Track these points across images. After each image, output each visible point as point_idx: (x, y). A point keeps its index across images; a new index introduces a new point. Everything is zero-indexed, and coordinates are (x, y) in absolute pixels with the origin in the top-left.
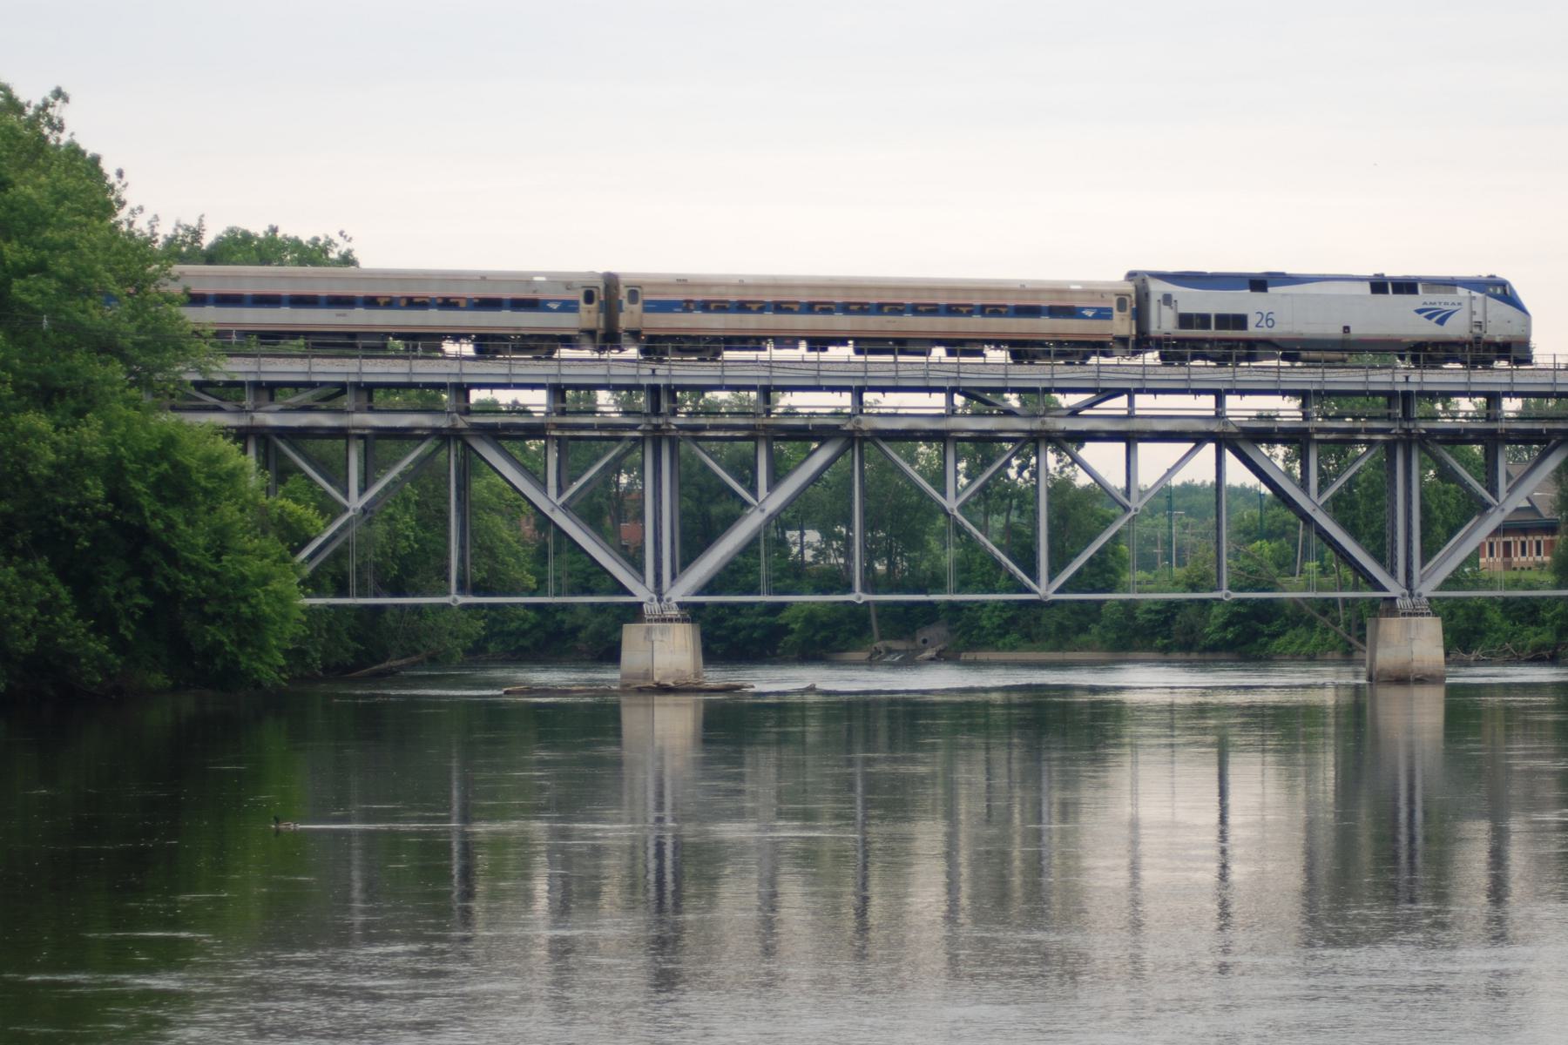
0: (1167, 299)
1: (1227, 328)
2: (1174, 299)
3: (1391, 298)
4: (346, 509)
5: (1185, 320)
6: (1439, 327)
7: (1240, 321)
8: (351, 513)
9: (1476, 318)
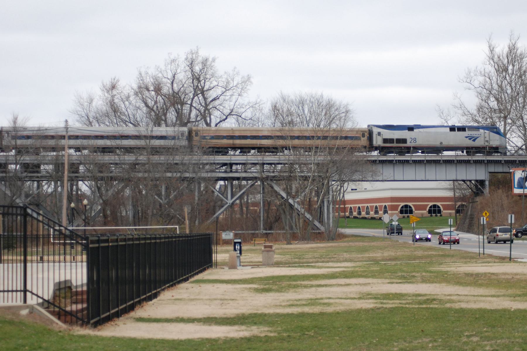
0: (379, 134)
1: (387, 143)
2: (381, 133)
3: (456, 133)
4: (227, 203)
5: (385, 141)
6: (473, 142)
7: (404, 141)
8: (228, 204)
9: (487, 139)
